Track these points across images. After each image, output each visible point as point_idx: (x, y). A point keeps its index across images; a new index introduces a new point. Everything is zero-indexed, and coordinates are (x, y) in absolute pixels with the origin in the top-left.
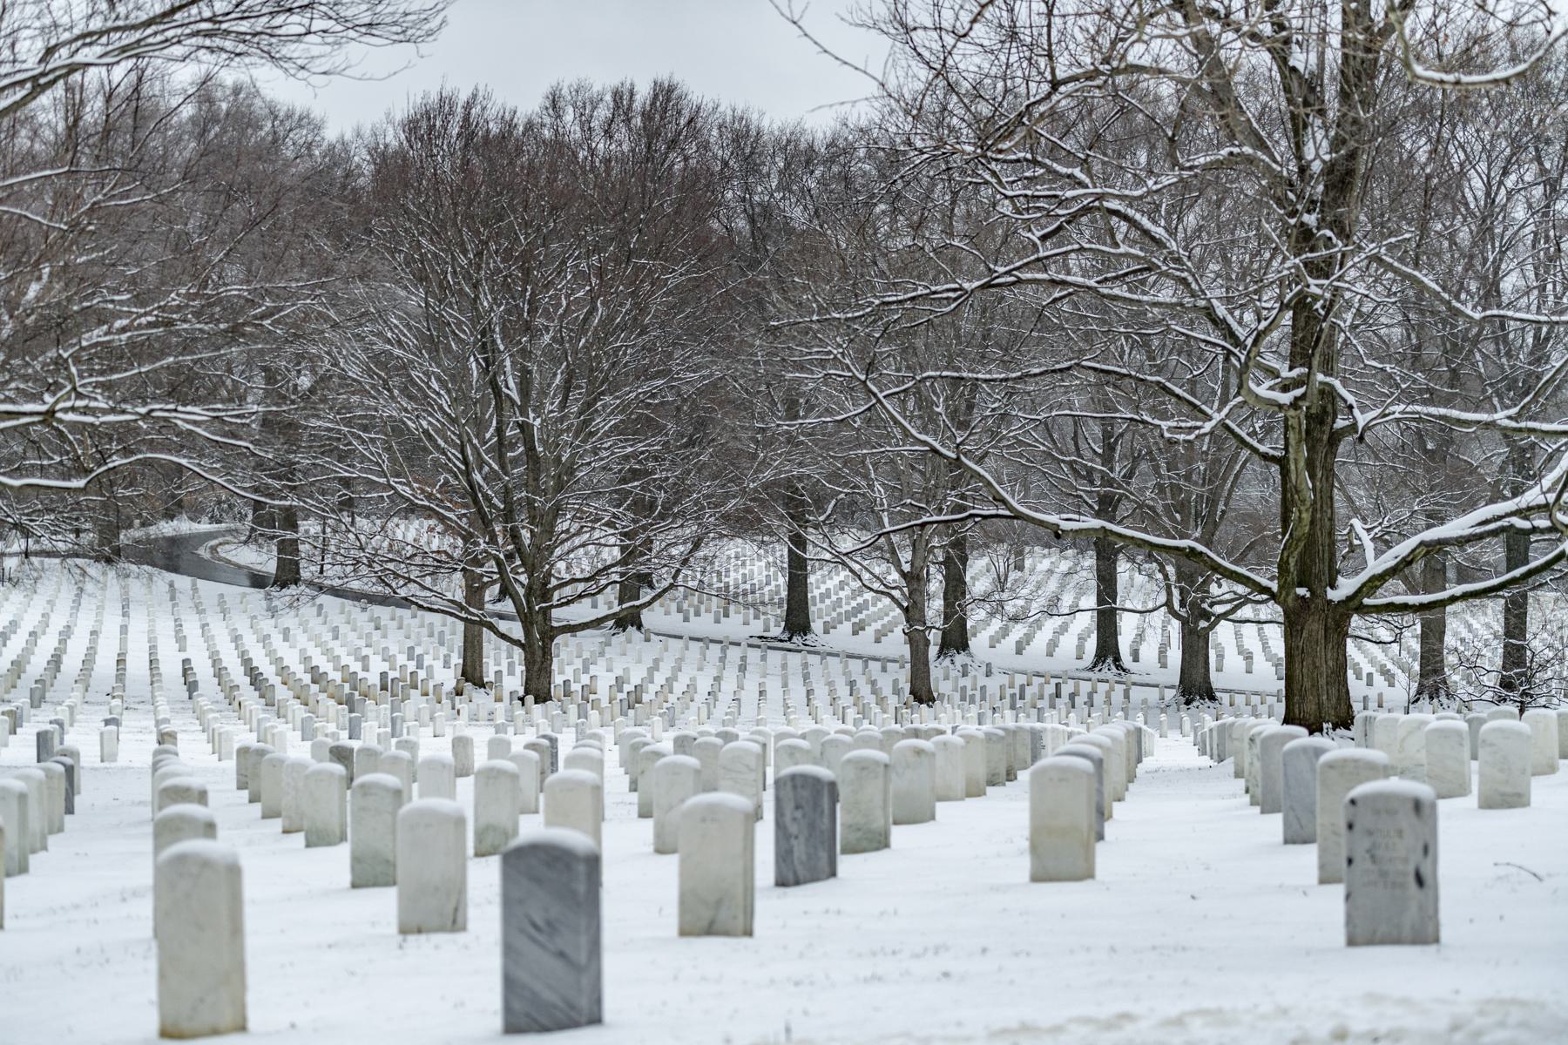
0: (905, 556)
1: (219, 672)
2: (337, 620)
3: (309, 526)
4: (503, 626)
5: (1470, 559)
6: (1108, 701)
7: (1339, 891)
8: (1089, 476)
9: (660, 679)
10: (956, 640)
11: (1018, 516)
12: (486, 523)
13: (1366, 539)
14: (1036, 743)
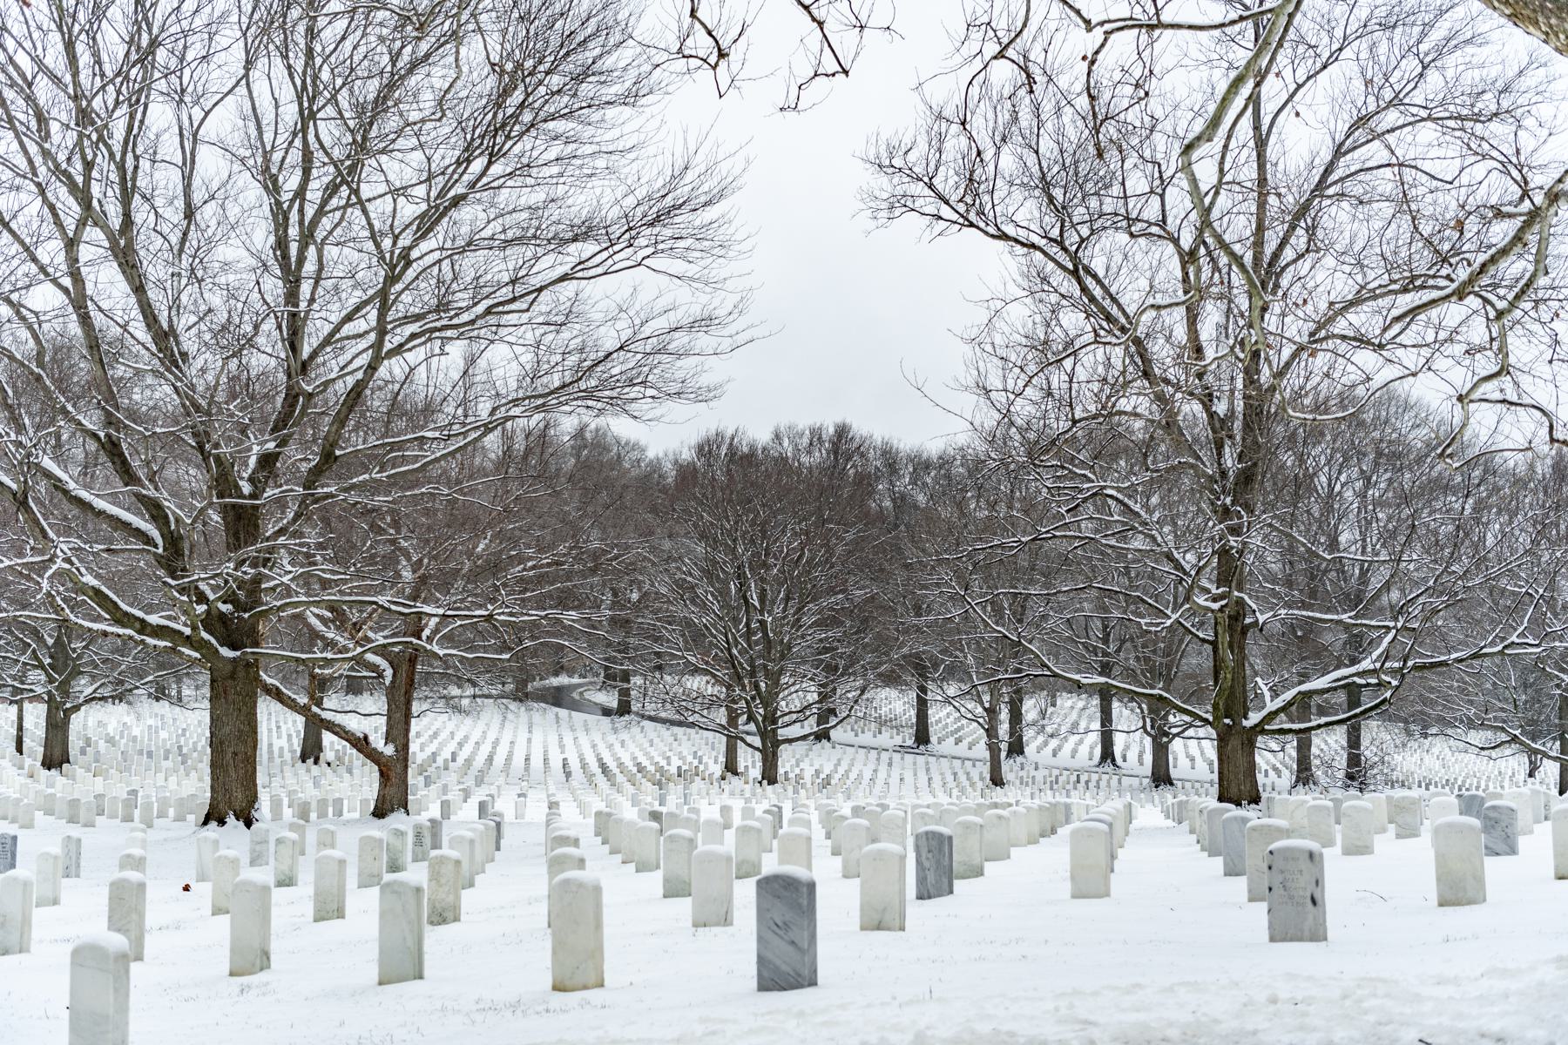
0: (986, 698)
1: (584, 766)
2: (652, 735)
3: (637, 680)
4: (749, 739)
5: (1326, 701)
6: (1109, 786)
7: (1264, 906)
8: (1095, 651)
9: (841, 770)
10: (1017, 748)
11: (1055, 675)
12: (740, 678)
13: (1265, 689)
14: (1068, 814)
